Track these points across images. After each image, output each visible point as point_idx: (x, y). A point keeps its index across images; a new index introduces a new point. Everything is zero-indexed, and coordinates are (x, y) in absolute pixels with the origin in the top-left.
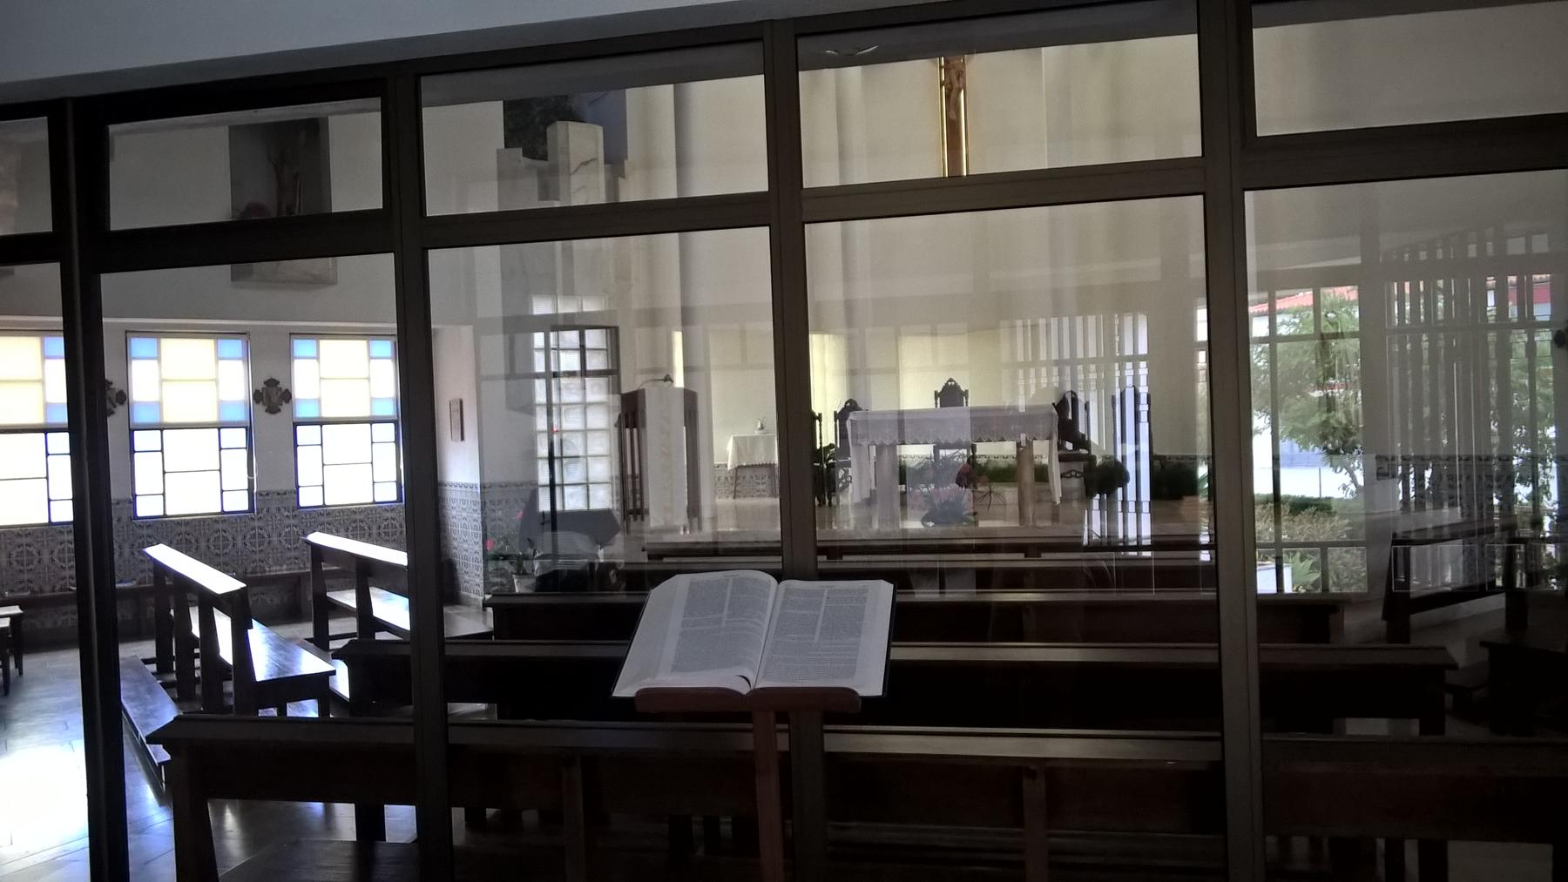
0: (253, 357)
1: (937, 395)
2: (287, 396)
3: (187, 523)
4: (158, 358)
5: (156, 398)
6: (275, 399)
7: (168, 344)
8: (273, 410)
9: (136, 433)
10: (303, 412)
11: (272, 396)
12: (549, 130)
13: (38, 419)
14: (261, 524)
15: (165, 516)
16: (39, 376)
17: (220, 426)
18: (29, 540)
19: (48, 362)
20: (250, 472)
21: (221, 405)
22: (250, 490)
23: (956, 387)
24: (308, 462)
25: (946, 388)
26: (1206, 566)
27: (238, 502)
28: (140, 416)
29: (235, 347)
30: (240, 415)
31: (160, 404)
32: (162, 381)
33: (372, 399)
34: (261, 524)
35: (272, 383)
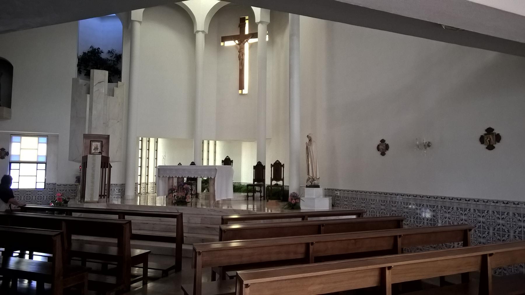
1: (223, 161)
4: (20, 142)
5: (18, 154)
7: (24, 138)
10: (13, 159)
12: (103, 59)
13: (35, 160)
14: (491, 229)
17: (37, 163)
18: (41, 193)
22: (45, 182)
23: (229, 159)
25: (226, 159)
26: (48, 290)
27: (41, 186)
29: (44, 140)
30: (43, 159)
31: (19, 156)
32: (21, 149)
33: (38, 156)
34: (491, 229)
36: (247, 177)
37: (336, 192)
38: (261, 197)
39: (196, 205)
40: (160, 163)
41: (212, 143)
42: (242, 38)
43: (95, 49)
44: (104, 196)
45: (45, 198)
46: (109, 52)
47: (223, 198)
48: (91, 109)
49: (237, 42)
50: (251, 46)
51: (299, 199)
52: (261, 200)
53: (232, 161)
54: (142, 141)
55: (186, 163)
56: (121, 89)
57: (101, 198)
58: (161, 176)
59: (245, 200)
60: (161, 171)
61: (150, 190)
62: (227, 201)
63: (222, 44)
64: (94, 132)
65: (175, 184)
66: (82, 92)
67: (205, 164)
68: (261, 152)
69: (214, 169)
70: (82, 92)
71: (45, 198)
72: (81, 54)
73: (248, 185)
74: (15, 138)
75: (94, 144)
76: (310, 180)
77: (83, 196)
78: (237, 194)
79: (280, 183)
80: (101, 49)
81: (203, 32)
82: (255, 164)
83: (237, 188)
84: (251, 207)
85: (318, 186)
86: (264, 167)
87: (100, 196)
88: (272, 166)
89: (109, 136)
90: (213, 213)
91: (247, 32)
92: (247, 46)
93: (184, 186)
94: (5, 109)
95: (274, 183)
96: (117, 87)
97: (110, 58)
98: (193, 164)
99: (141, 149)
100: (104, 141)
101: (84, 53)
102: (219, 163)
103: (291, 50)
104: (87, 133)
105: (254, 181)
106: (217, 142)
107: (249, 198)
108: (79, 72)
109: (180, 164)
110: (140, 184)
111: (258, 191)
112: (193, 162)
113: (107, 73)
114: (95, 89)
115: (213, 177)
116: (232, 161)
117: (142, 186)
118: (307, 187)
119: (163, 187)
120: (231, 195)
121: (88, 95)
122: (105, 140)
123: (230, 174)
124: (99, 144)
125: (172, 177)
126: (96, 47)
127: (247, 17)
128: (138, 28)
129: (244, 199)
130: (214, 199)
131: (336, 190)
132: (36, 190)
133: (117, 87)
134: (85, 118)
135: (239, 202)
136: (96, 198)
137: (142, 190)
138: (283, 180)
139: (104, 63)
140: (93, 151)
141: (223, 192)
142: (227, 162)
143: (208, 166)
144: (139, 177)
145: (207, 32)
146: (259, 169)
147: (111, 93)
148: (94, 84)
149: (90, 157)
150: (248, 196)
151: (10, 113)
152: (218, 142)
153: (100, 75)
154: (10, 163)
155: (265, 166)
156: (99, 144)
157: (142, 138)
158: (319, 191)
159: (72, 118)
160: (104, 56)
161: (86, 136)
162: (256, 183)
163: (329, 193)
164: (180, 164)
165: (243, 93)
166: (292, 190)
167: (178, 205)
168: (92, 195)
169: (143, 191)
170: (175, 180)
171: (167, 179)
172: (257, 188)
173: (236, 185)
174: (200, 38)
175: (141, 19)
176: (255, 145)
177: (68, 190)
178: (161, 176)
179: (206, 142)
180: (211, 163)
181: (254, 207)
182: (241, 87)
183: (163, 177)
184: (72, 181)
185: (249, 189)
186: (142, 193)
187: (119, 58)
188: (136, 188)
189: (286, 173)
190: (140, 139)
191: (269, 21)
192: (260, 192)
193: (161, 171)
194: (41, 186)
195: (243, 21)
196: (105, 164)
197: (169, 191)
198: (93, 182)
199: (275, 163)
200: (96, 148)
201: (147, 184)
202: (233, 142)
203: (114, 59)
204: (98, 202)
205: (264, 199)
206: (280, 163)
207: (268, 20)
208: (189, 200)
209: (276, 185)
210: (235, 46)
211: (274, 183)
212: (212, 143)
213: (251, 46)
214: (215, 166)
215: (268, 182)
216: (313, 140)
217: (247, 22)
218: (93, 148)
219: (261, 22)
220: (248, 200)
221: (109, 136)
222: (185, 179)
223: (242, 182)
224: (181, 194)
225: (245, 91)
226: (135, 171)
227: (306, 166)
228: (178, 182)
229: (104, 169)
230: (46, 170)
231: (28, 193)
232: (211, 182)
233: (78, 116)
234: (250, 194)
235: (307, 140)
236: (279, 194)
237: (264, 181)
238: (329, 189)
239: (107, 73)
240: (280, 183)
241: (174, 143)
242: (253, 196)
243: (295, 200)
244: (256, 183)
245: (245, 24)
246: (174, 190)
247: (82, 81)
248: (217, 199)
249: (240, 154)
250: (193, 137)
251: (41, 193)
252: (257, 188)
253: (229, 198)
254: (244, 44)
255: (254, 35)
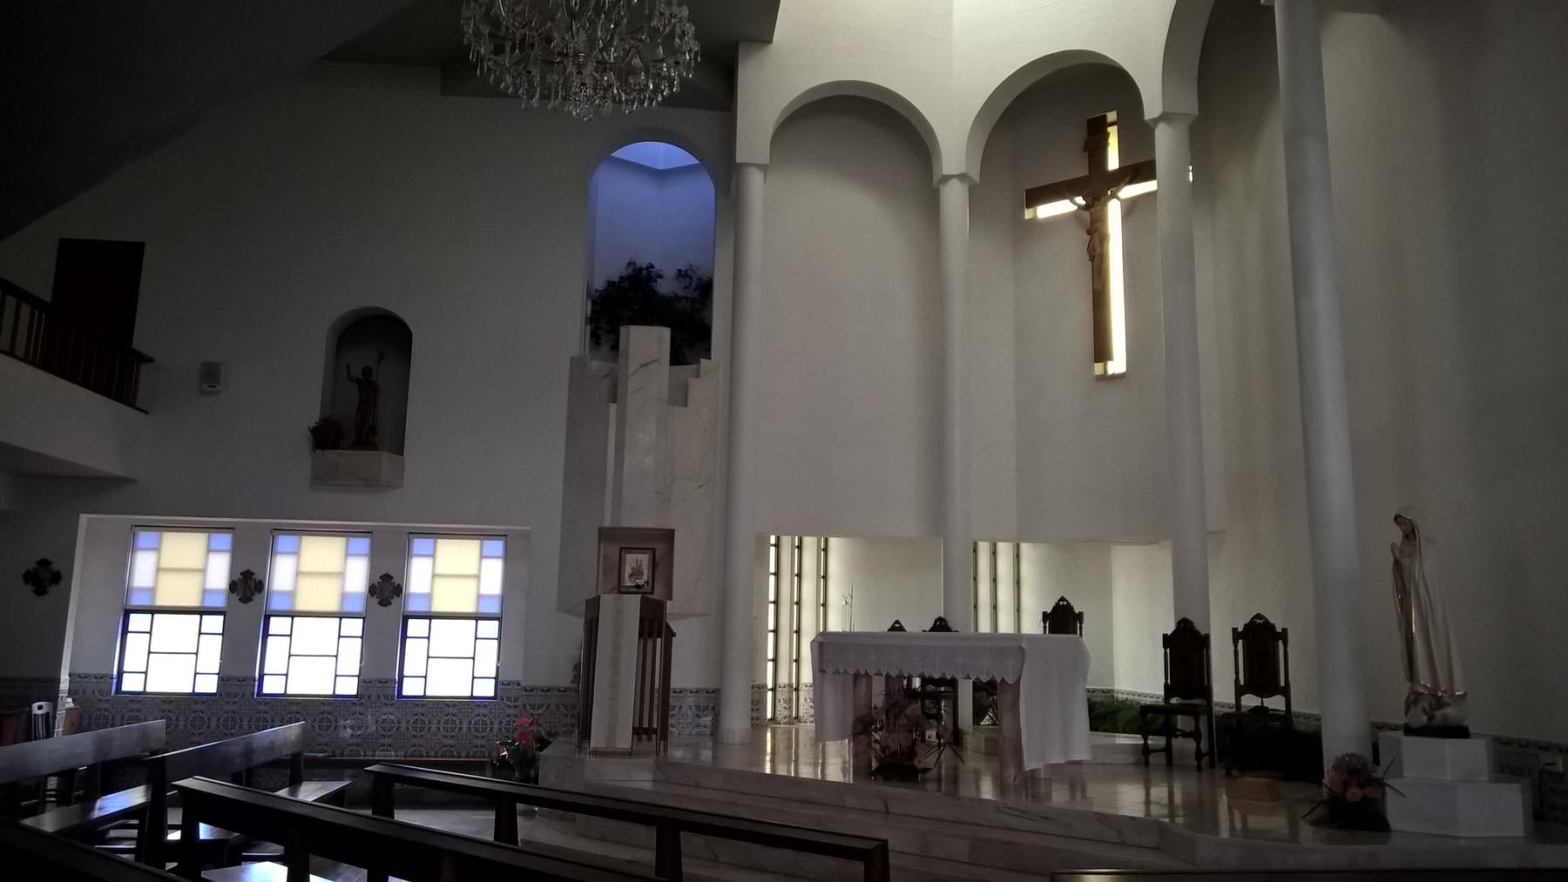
0: (374, 557)
1: (1045, 616)
2: (260, 587)
3: (298, 703)
6: (386, 594)
8: (385, 603)
9: (411, 622)
11: (386, 588)
13: (470, 608)
15: (285, 695)
16: (474, 571)
18: (485, 711)
19: (485, 561)
20: (1237, 673)
21: (344, 596)
22: (496, 678)
23: (1069, 608)
24: (414, 654)
25: (1057, 608)
27: (486, 689)
28: (276, 605)
30: (359, 607)
32: (434, 576)
35: (386, 578)
36: (1138, 673)
37: (1547, 757)
38: (1199, 754)
39: (955, 780)
40: (835, 624)
41: (1004, 549)
42: (1096, 186)
43: (641, 269)
44: (649, 732)
45: (496, 726)
46: (681, 274)
47: (1054, 761)
48: (620, 449)
49: (1080, 200)
50: (1130, 207)
51: (1380, 784)
52: (1199, 769)
53: (1080, 617)
54: (777, 545)
55: (918, 623)
56: (708, 376)
57: (640, 740)
58: (830, 670)
59: (1136, 764)
60: (827, 645)
61: (806, 708)
62: (1073, 774)
63: (1028, 214)
64: (629, 522)
65: (879, 700)
66: (598, 393)
67: (985, 627)
68: (1189, 584)
69: (1015, 646)
70: (598, 393)
71: (496, 726)
72: (599, 284)
73: (1146, 709)
74: (419, 544)
75: (631, 559)
76: (1425, 704)
77: (586, 734)
78: (1102, 738)
79: (1275, 703)
80: (657, 266)
81: (962, 177)
82: (1170, 630)
83: (1107, 713)
84: (1159, 792)
85: (1460, 732)
86: (1204, 641)
87: (638, 732)
88: (1237, 636)
89: (672, 532)
90: (1014, 822)
91: (1113, 163)
92: (1114, 211)
93: (910, 707)
94: (386, 457)
95: (1250, 701)
96: (698, 375)
97: (681, 293)
98: (941, 625)
99: (777, 574)
100: (660, 548)
101: (611, 284)
102: (1032, 625)
103: (1296, 191)
104: (607, 524)
105: (1169, 690)
106: (1024, 547)
107: (1153, 759)
108: (595, 338)
109: (897, 627)
110: (774, 690)
111: (1185, 735)
112: (940, 619)
113: (666, 333)
114: (632, 384)
115: (1010, 680)
116: (1080, 617)
117: (779, 696)
118: (1409, 730)
119: (840, 710)
120: (1082, 744)
121: (613, 407)
122: (661, 543)
123: (1079, 661)
124: (644, 558)
125: (867, 674)
126: (642, 262)
127: (1112, 116)
128: (756, 186)
129: (1131, 759)
130: (1020, 765)
131: (1547, 748)
132: (473, 702)
133: (698, 375)
134: (604, 477)
135: (1111, 773)
136: (624, 741)
137: (779, 708)
138: (1285, 692)
139: (663, 308)
140: (628, 582)
141: (1055, 737)
142: (1062, 619)
143: (995, 636)
144: (770, 665)
145: (977, 179)
146: (1185, 649)
147: (680, 396)
148: (631, 369)
149: (607, 601)
150: (1146, 750)
151: (400, 471)
152: (1025, 548)
153: (648, 342)
154: (406, 619)
155: (1207, 637)
156: (644, 558)
157: (778, 539)
158: (1471, 754)
159: (568, 478)
160: (665, 287)
161: (605, 535)
162: (1174, 701)
163: (1512, 760)
164: (897, 627)
165: (1110, 372)
166: (1341, 739)
167: (886, 779)
168: (612, 729)
169: (782, 712)
170: (878, 686)
171: (851, 679)
172: (1182, 722)
173: (1098, 698)
174: (955, 199)
175: (763, 156)
176: (1161, 558)
177: (553, 707)
178: (830, 670)
179: (984, 548)
180: (1006, 626)
181: (1171, 794)
182: (1102, 352)
183: (837, 672)
184: (564, 678)
185: (1144, 718)
186: (779, 717)
187: (705, 289)
188: (758, 704)
189: (1296, 664)
190: (773, 540)
191: (1196, 112)
192: (1195, 735)
193: (827, 645)
194: (486, 689)
195: (1097, 132)
196: (654, 625)
197: (855, 725)
198: (614, 686)
199: (1250, 626)
200: (636, 573)
201: (797, 689)
202: (1081, 545)
203: (695, 295)
204: (630, 754)
205: (1212, 765)
206: (1269, 627)
207: (1189, 104)
208: (926, 760)
209: (1261, 711)
210: (1074, 215)
211: (1250, 701)
212: (1004, 549)
213: (1130, 207)
214: (1018, 637)
215: (1223, 691)
216: (1423, 531)
217: (1113, 132)
218: (628, 570)
219: (1165, 117)
220: (1147, 764)
221: (672, 532)
222: (917, 683)
223: (1116, 687)
224: (897, 741)
225: (1118, 364)
226: (756, 649)
227: (1398, 643)
228: (888, 694)
229: (650, 645)
230: (499, 639)
231: (451, 710)
232: (1004, 699)
233: (585, 471)
234: (1156, 741)
235: (1397, 535)
236: (1266, 748)
237: (1206, 692)
238: (1507, 742)
239: (666, 333)
240: (1275, 703)
241: (881, 555)
242: (1168, 749)
243: (1362, 786)
244: (1174, 701)
245: (1107, 135)
246: (873, 722)
247: (597, 365)
248: (1029, 765)
249: (1105, 590)
250: (938, 532)
251: (485, 711)
252: (1182, 722)
253: (1076, 757)
254: (1105, 205)
255: (1138, 170)
